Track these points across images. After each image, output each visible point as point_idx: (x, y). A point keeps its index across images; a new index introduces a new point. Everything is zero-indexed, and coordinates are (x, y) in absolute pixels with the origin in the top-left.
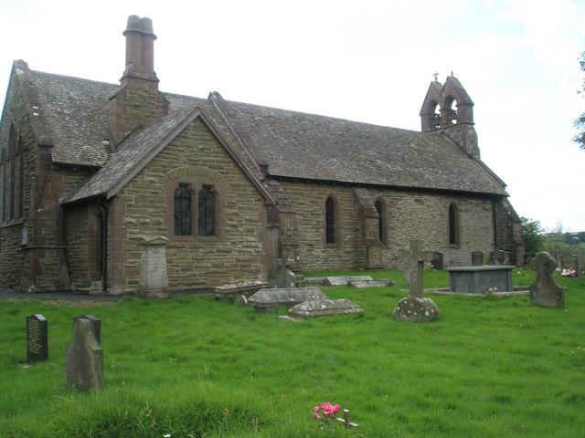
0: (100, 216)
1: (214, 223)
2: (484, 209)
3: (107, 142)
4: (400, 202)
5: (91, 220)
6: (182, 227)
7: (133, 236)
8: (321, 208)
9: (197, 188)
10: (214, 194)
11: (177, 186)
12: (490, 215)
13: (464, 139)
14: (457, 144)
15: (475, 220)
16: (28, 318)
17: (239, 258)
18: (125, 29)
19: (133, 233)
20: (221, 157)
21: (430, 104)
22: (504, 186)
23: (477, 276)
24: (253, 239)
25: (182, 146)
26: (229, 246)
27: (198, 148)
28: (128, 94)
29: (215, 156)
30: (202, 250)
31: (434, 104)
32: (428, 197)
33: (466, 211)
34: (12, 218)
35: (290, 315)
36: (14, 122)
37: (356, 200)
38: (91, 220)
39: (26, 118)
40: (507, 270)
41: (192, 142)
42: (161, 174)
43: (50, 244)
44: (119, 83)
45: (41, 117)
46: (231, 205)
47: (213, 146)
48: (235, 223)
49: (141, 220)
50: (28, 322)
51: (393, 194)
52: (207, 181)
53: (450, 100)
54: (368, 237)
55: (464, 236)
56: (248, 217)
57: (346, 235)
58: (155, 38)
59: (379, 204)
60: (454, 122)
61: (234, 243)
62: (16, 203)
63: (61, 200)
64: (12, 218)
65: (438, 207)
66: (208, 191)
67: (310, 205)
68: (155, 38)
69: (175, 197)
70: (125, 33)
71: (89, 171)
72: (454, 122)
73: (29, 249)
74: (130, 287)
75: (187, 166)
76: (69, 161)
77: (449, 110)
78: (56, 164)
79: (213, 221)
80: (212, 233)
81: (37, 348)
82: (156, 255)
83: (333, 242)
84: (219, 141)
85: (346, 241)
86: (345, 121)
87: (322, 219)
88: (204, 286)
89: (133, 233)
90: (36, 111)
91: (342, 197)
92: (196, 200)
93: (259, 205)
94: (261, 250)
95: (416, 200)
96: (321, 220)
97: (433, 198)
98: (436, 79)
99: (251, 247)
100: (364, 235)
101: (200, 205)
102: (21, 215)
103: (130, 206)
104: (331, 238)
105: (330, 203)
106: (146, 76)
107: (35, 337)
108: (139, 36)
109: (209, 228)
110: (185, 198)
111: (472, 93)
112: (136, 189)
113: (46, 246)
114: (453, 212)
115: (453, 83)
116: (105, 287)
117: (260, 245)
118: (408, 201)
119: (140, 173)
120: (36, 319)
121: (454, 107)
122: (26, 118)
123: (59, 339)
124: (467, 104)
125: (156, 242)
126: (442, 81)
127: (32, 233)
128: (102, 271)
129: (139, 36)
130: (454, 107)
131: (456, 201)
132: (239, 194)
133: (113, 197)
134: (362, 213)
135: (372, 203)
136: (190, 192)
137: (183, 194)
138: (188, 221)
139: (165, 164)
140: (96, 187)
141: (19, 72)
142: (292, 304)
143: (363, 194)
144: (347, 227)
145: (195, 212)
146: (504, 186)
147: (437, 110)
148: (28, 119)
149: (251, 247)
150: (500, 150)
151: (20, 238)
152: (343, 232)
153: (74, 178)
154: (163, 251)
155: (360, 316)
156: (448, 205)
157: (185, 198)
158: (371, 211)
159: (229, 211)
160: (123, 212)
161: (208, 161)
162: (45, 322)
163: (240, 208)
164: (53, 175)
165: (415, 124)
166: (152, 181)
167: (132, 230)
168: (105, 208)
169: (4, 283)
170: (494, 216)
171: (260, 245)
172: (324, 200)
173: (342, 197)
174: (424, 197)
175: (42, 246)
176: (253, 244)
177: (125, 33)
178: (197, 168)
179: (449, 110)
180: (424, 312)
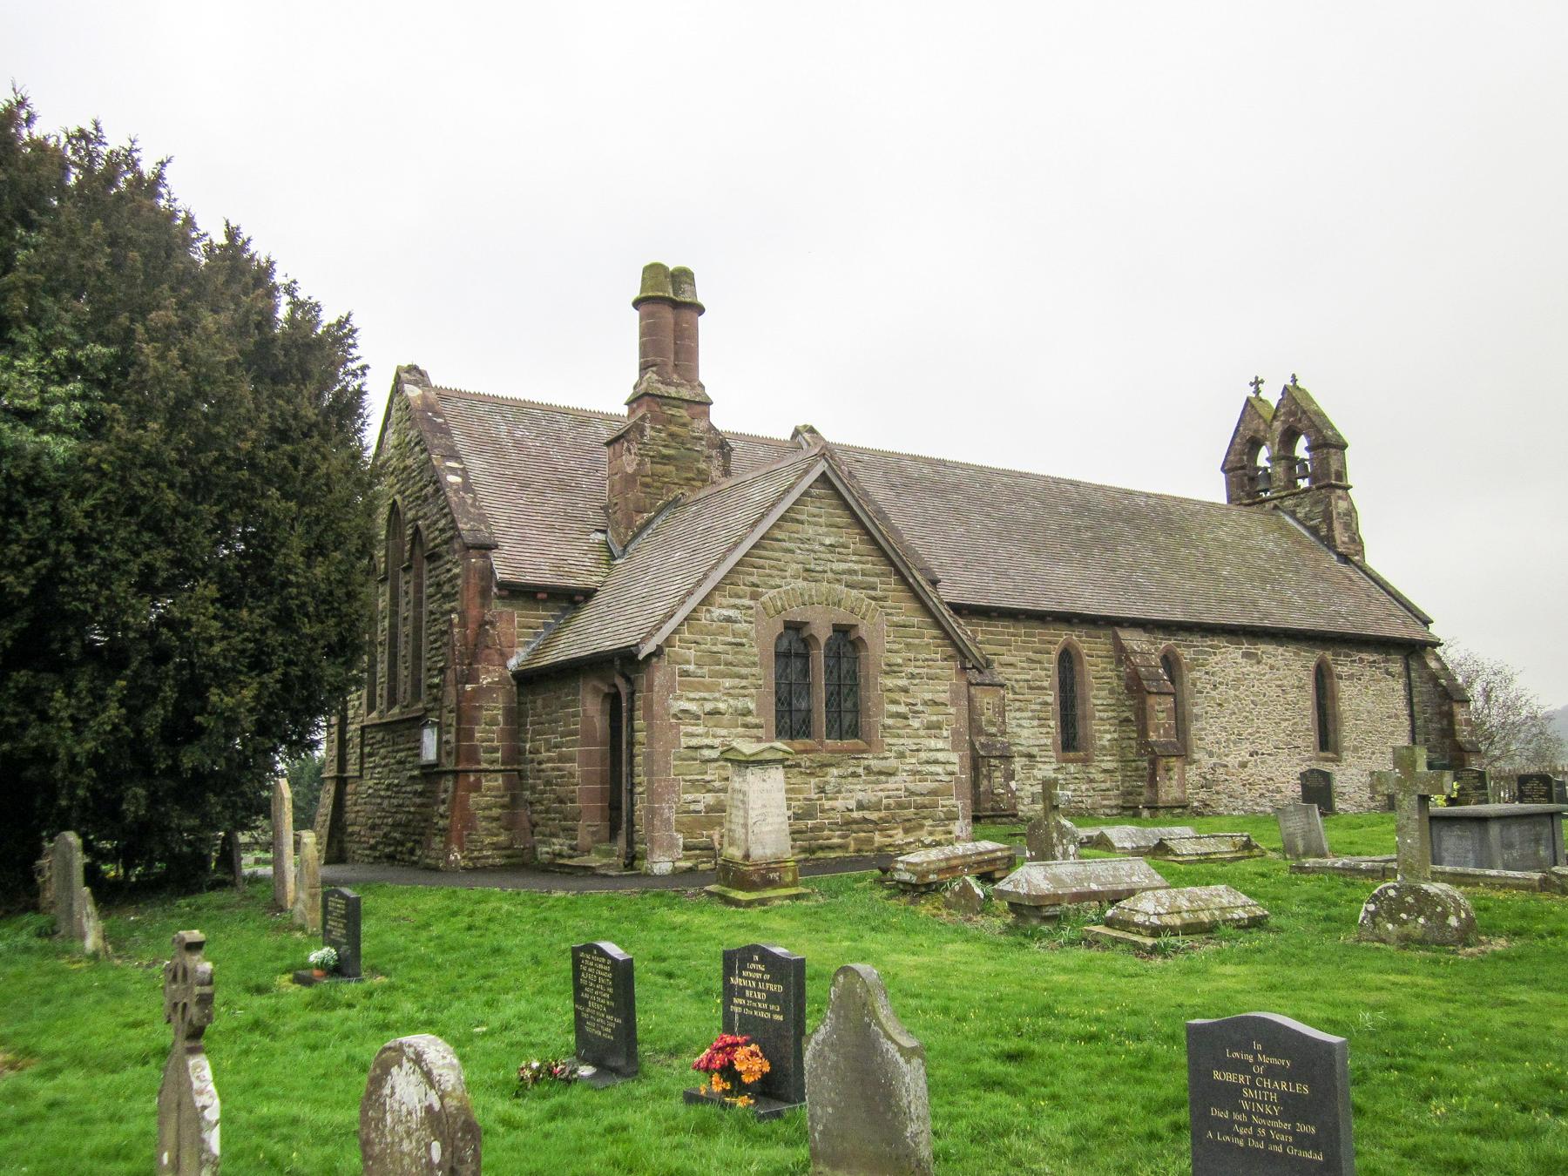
0: (613, 700)
1: (856, 710)
2: (1389, 673)
3: (601, 537)
4: (1213, 659)
5: (589, 707)
6: (791, 720)
7: (694, 742)
8: (1047, 674)
9: (823, 633)
10: (857, 644)
11: (780, 629)
12: (1399, 686)
13: (1328, 518)
14: (1314, 531)
15: (1373, 701)
16: (575, 951)
17: (911, 786)
18: (636, 293)
19: (692, 735)
20: (872, 564)
21: (1246, 443)
22: (1427, 622)
23: (1494, 830)
24: (940, 745)
25: (791, 540)
26: (893, 763)
27: (822, 544)
28: (648, 432)
29: (858, 561)
30: (835, 771)
31: (1255, 444)
32: (1270, 648)
33: (1351, 677)
34: (392, 702)
35: (1110, 923)
36: (398, 497)
37: (1121, 654)
38: (589, 707)
39: (430, 489)
40: (1552, 815)
41: (810, 531)
42: (747, 602)
43: (492, 762)
44: (625, 411)
45: (467, 486)
46: (892, 670)
47: (854, 539)
48: (902, 709)
49: (709, 706)
50: (577, 962)
51: (1197, 640)
52: (845, 618)
53: (1290, 437)
54: (1153, 737)
55: (1349, 734)
56: (928, 696)
57: (1103, 731)
58: (700, 310)
59: (1170, 663)
60: (1304, 484)
61: (901, 755)
62: (403, 673)
63: (513, 663)
64: (392, 702)
65: (1289, 670)
66: (846, 639)
67: (1025, 665)
68: (700, 310)
69: (777, 655)
70: (637, 304)
71: (571, 599)
72: (1304, 484)
73: (446, 773)
74: (687, 858)
75: (800, 583)
76: (529, 579)
77: (1288, 458)
78: (503, 585)
79: (855, 705)
80: (854, 731)
81: (604, 1027)
82: (766, 786)
83: (1075, 749)
84: (868, 533)
85: (1104, 747)
86: (1075, 484)
87: (1051, 697)
88: (839, 854)
89: (692, 735)
90: (453, 471)
91: (1093, 652)
92: (819, 657)
93: (949, 670)
94: (956, 769)
95: (1246, 655)
96: (1050, 699)
97: (1281, 650)
98: (1257, 391)
99: (936, 762)
100: (1143, 732)
101: (829, 671)
102: (416, 696)
103: (685, 674)
104: (1071, 739)
105: (1068, 661)
106: (685, 393)
107: (601, 999)
108: (668, 306)
109: (847, 719)
110: (797, 655)
111: (1342, 421)
112: (698, 637)
113: (485, 766)
114: (1323, 681)
115: (1294, 398)
116: (632, 859)
117: (954, 757)
118: (1228, 658)
119: (706, 601)
120: (602, 953)
121: (1301, 449)
122: (430, 489)
123: (677, 1014)
124: (1329, 445)
125: (768, 756)
126: (1272, 395)
127: (451, 737)
128: (617, 811)
129: (668, 306)
130: (1301, 449)
131: (1329, 656)
132: (907, 645)
133: (650, 656)
134: (1135, 688)
135: (1155, 660)
136: (808, 642)
137: (794, 645)
138: (803, 706)
139: (754, 579)
140: (591, 634)
141: (413, 392)
142: (1115, 898)
143: (1135, 641)
144: (1104, 715)
145: (818, 689)
146: (1427, 622)
147: (1263, 459)
148: (437, 490)
149: (936, 762)
150: (1418, 540)
151: (417, 749)
152: (1095, 726)
153: (541, 616)
154: (777, 774)
155: (1256, 923)
156: (1312, 664)
157: (797, 655)
158: (1158, 679)
159: (890, 682)
160: (671, 689)
161: (844, 572)
162: (629, 963)
163: (913, 676)
164: (497, 607)
165: (1215, 490)
166: (728, 619)
167: (690, 729)
168: (629, 680)
169: (373, 848)
170: (1409, 687)
171: (954, 757)
172: (1054, 656)
173: (1093, 652)
174: (1263, 647)
175: (475, 767)
176: (941, 756)
177: (637, 304)
178: (824, 581)
179: (1288, 458)
180: (1445, 915)
